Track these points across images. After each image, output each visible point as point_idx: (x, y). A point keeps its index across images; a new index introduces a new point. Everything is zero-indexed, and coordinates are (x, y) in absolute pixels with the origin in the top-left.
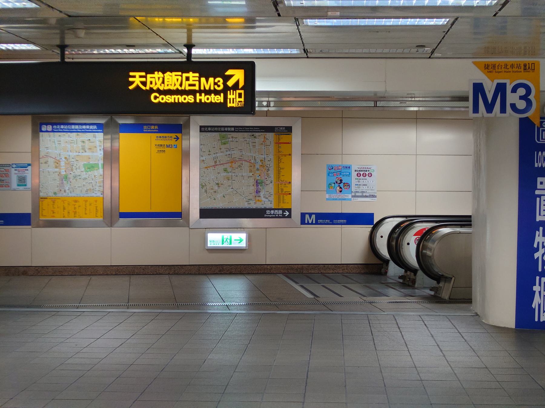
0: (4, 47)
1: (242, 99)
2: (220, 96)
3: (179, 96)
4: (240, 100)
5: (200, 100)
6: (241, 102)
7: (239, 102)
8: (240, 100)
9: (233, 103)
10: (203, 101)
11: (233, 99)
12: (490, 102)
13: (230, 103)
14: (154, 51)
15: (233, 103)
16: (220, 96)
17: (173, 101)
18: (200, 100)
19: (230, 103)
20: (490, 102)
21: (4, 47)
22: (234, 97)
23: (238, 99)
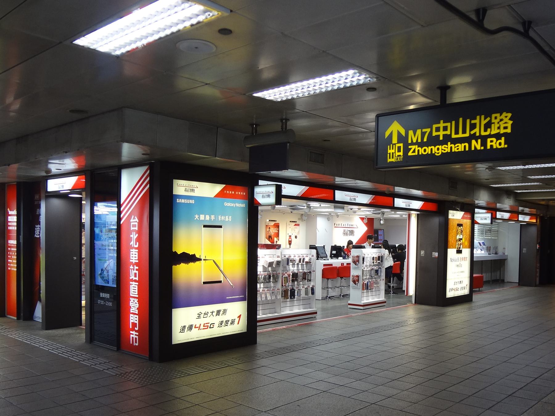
0: (553, 176)
1: (401, 153)
2: (447, 145)
3: (433, 147)
4: (399, 154)
5: (491, 146)
6: (400, 156)
7: (398, 156)
8: (399, 154)
9: (393, 158)
10: (495, 147)
11: (393, 153)
12: (82, 42)
13: (390, 158)
14: (83, 293)
15: (393, 158)
16: (447, 145)
17: (449, 151)
18: (491, 146)
19: (390, 158)
20: (82, 42)
21: (553, 176)
22: (393, 151)
23: (397, 154)
